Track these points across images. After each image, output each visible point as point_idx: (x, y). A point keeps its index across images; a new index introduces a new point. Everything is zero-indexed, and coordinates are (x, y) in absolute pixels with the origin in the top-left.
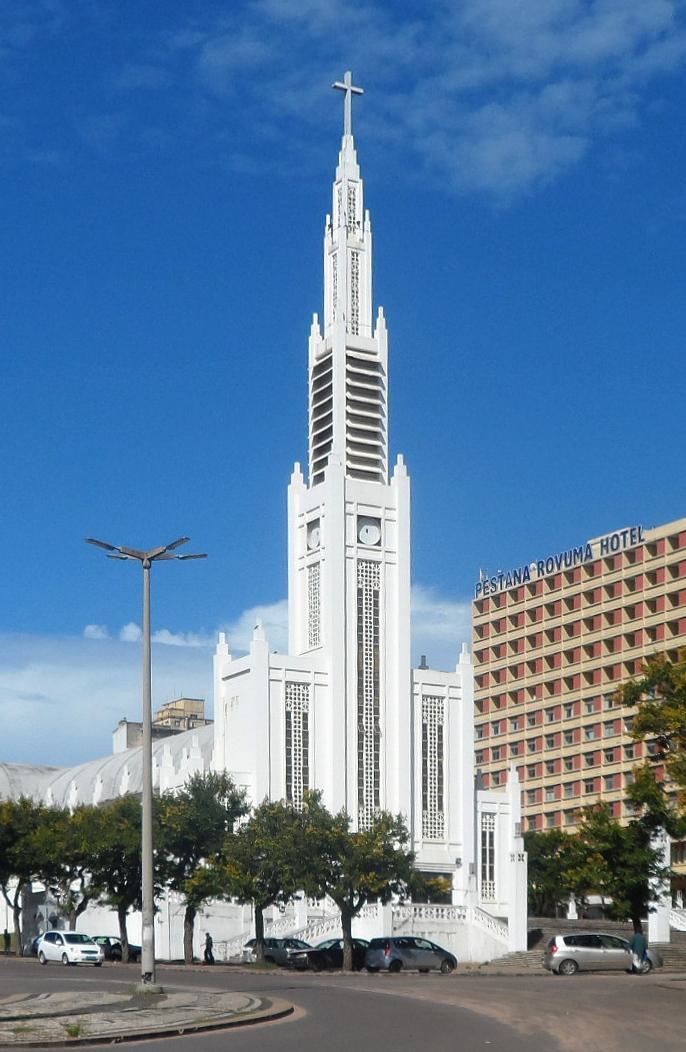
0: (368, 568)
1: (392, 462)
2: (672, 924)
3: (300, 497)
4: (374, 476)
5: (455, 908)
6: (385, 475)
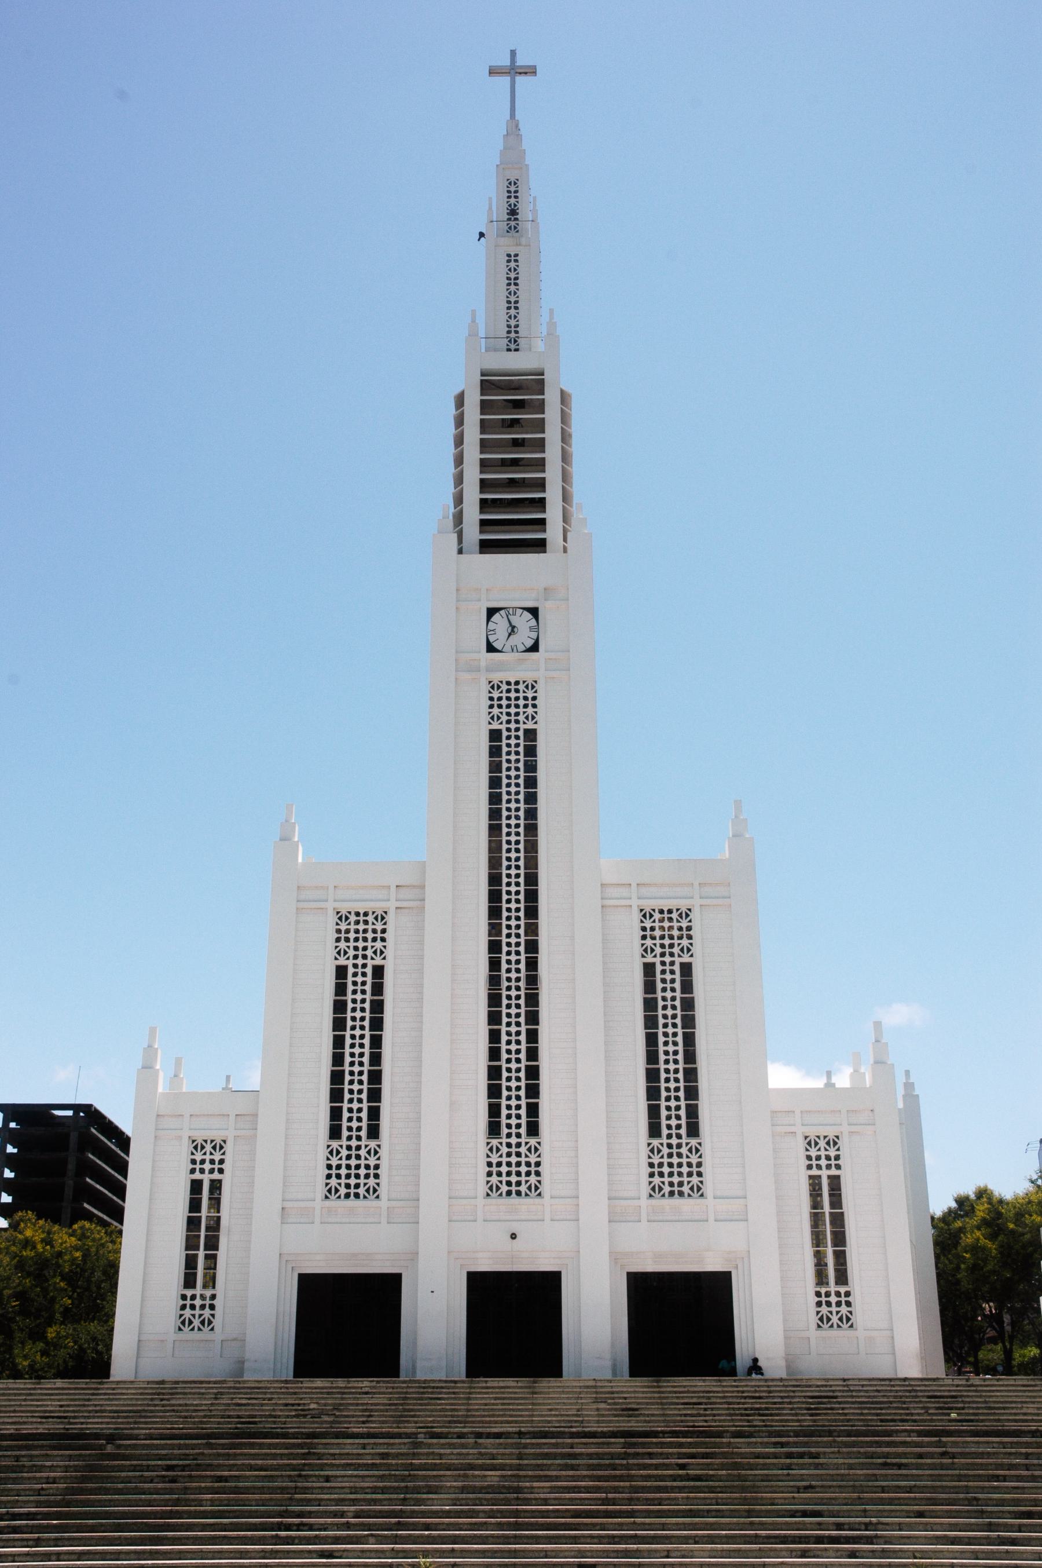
4: (539, 546)
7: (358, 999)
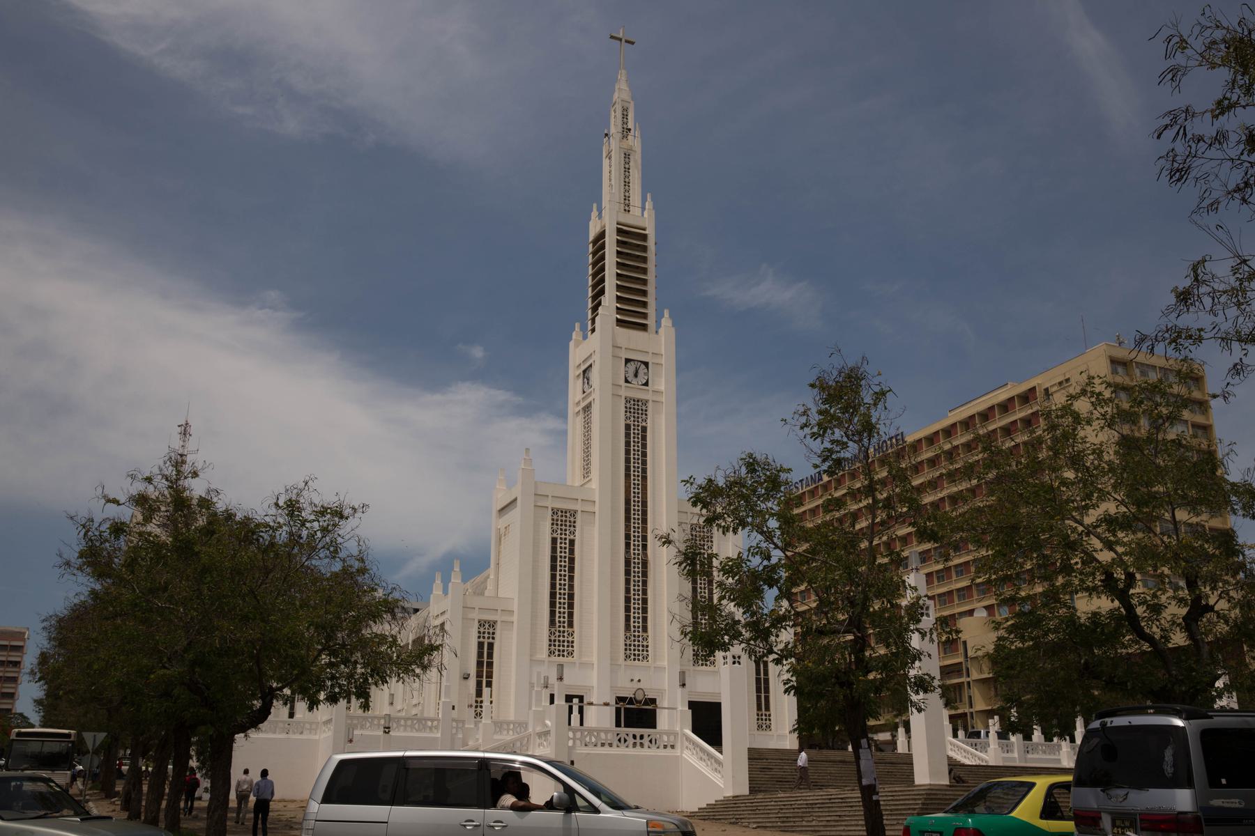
0: (636, 410)
1: (659, 317)
2: (951, 754)
3: (578, 352)
4: (644, 327)
5: (661, 734)
6: (651, 322)
7: (635, 614)
